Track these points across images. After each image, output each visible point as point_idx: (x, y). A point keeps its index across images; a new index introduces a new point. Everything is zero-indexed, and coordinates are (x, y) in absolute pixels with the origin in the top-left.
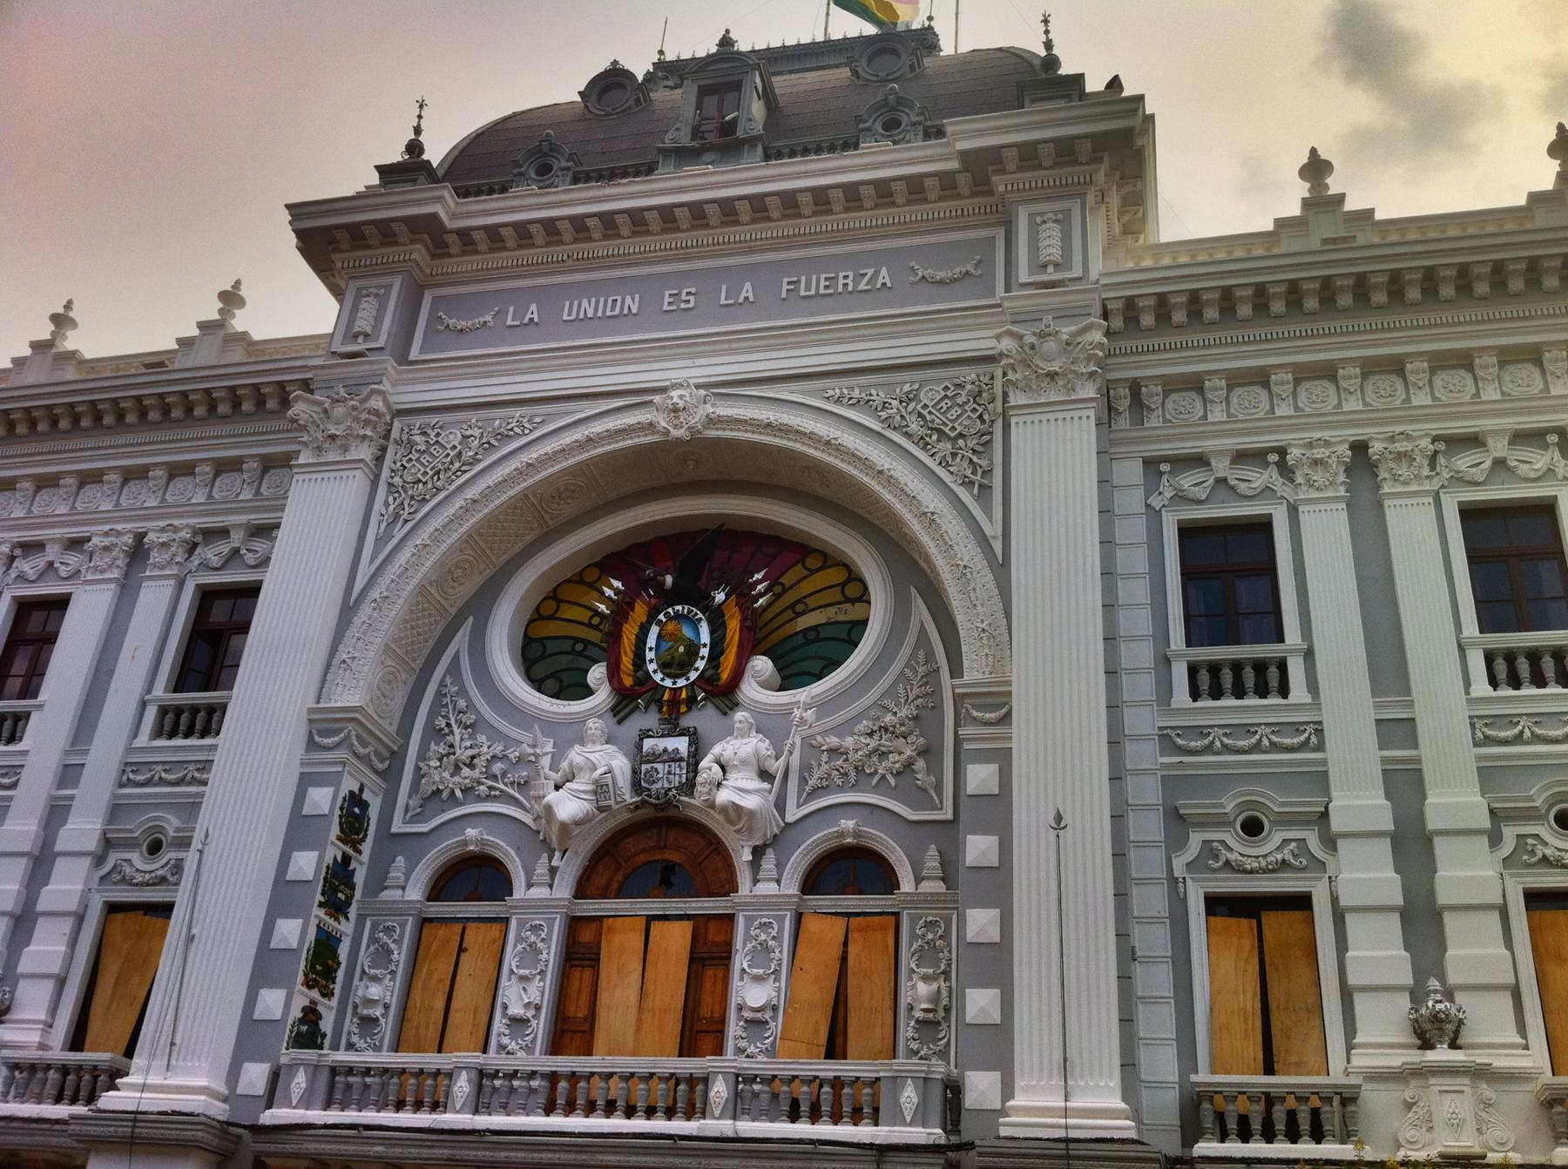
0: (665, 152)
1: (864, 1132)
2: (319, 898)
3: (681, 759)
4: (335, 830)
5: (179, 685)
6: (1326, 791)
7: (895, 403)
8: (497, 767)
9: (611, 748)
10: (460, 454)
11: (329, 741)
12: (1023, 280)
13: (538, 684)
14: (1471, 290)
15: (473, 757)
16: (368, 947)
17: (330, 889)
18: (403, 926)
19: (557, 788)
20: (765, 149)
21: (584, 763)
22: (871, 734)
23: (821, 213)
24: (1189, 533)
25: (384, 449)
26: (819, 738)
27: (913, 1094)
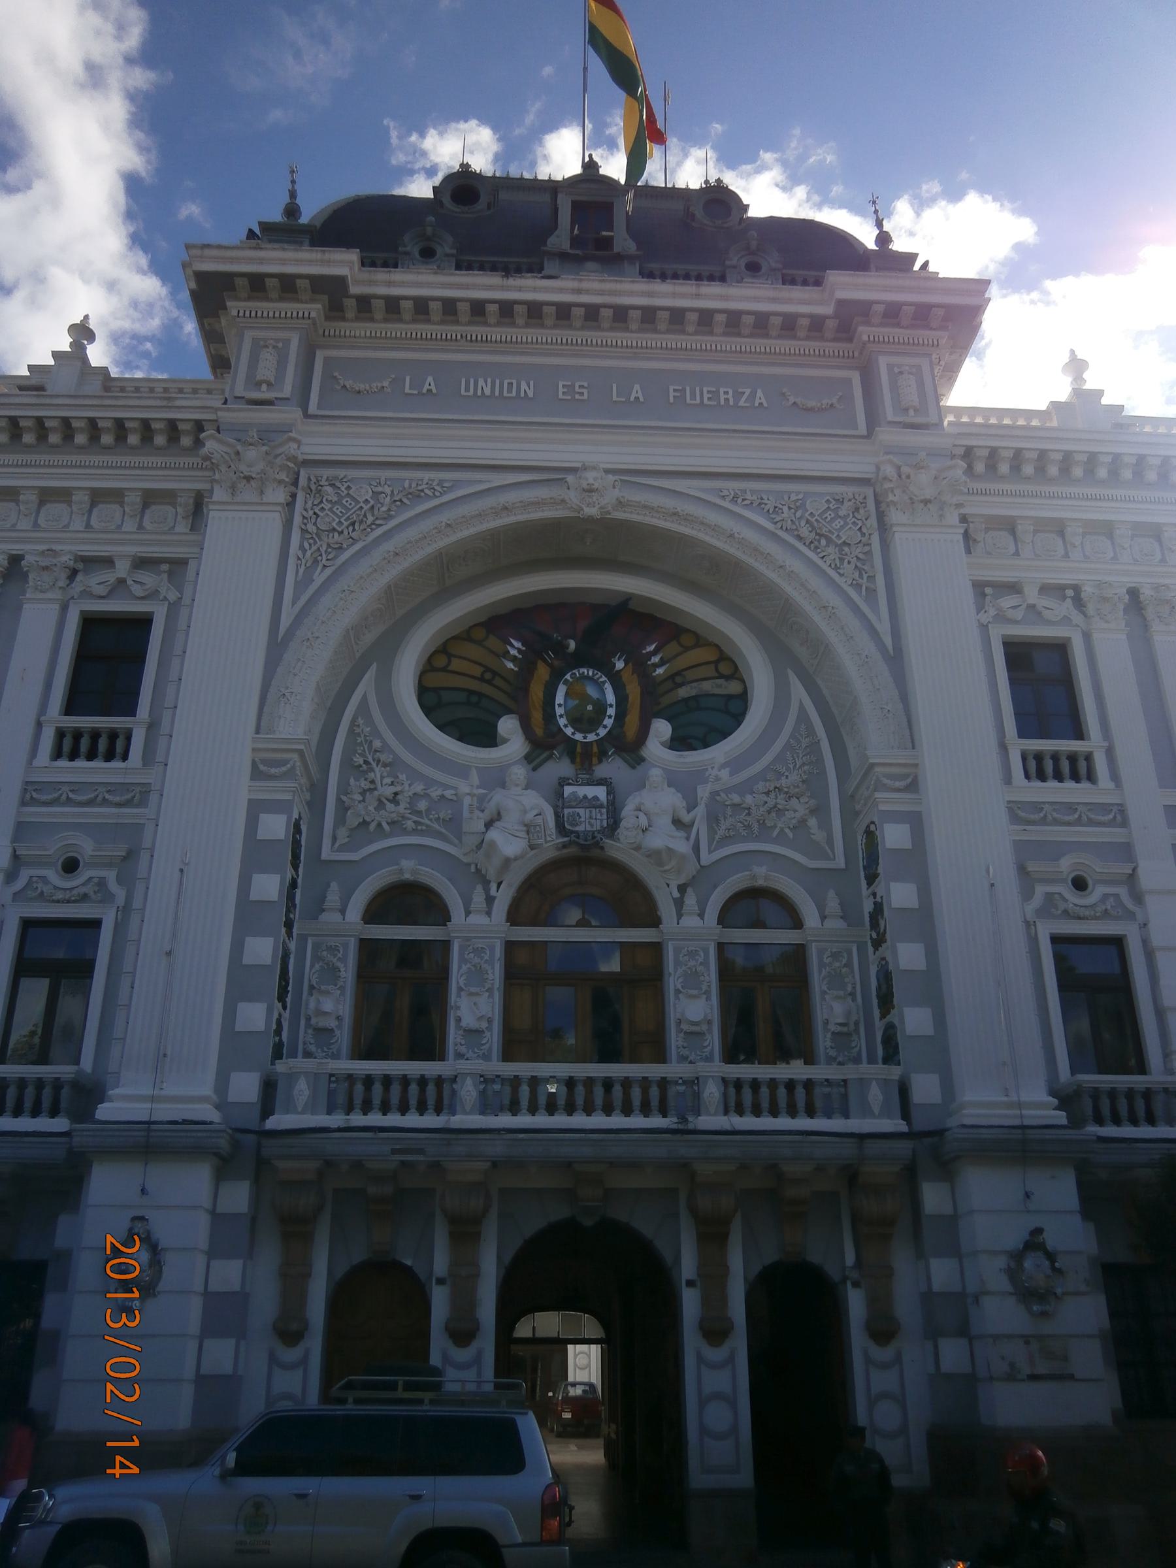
1: (836, 1124)
3: (601, 806)
5: (70, 708)
11: (273, 771)
15: (396, 794)
20: (783, 275)
22: (767, 793)
24: (90, 623)
25: (294, 496)
26: (723, 795)
27: (879, 1093)
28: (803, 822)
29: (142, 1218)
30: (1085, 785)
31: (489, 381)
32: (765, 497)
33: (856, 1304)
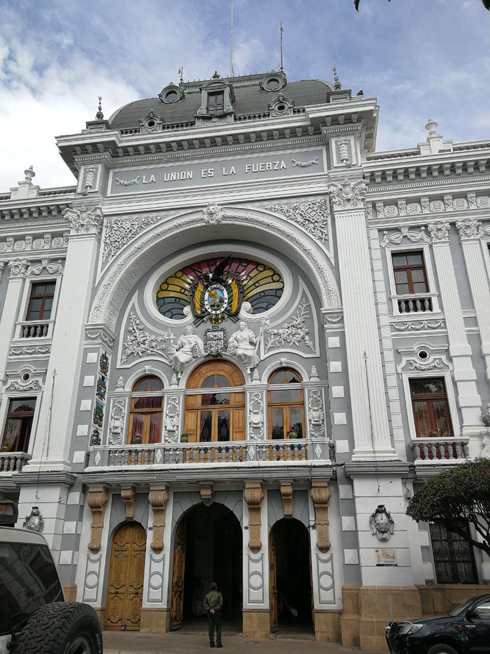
0: (198, 118)
2: (96, 392)
4: (99, 368)
5: (28, 318)
6: (448, 342)
7: (291, 210)
8: (154, 344)
9: (195, 336)
10: (131, 231)
12: (335, 165)
13: (164, 314)
14: (467, 170)
15: (144, 341)
16: (113, 409)
17: (99, 389)
18: (125, 401)
19: (177, 350)
20: (235, 117)
21: (188, 341)
22: (288, 328)
23: (270, 139)
24: (35, 285)
25: (101, 230)
26: (270, 330)
28: (303, 338)
29: (37, 508)
30: (428, 312)
31: (175, 173)
32: (283, 206)
33: (314, 538)
